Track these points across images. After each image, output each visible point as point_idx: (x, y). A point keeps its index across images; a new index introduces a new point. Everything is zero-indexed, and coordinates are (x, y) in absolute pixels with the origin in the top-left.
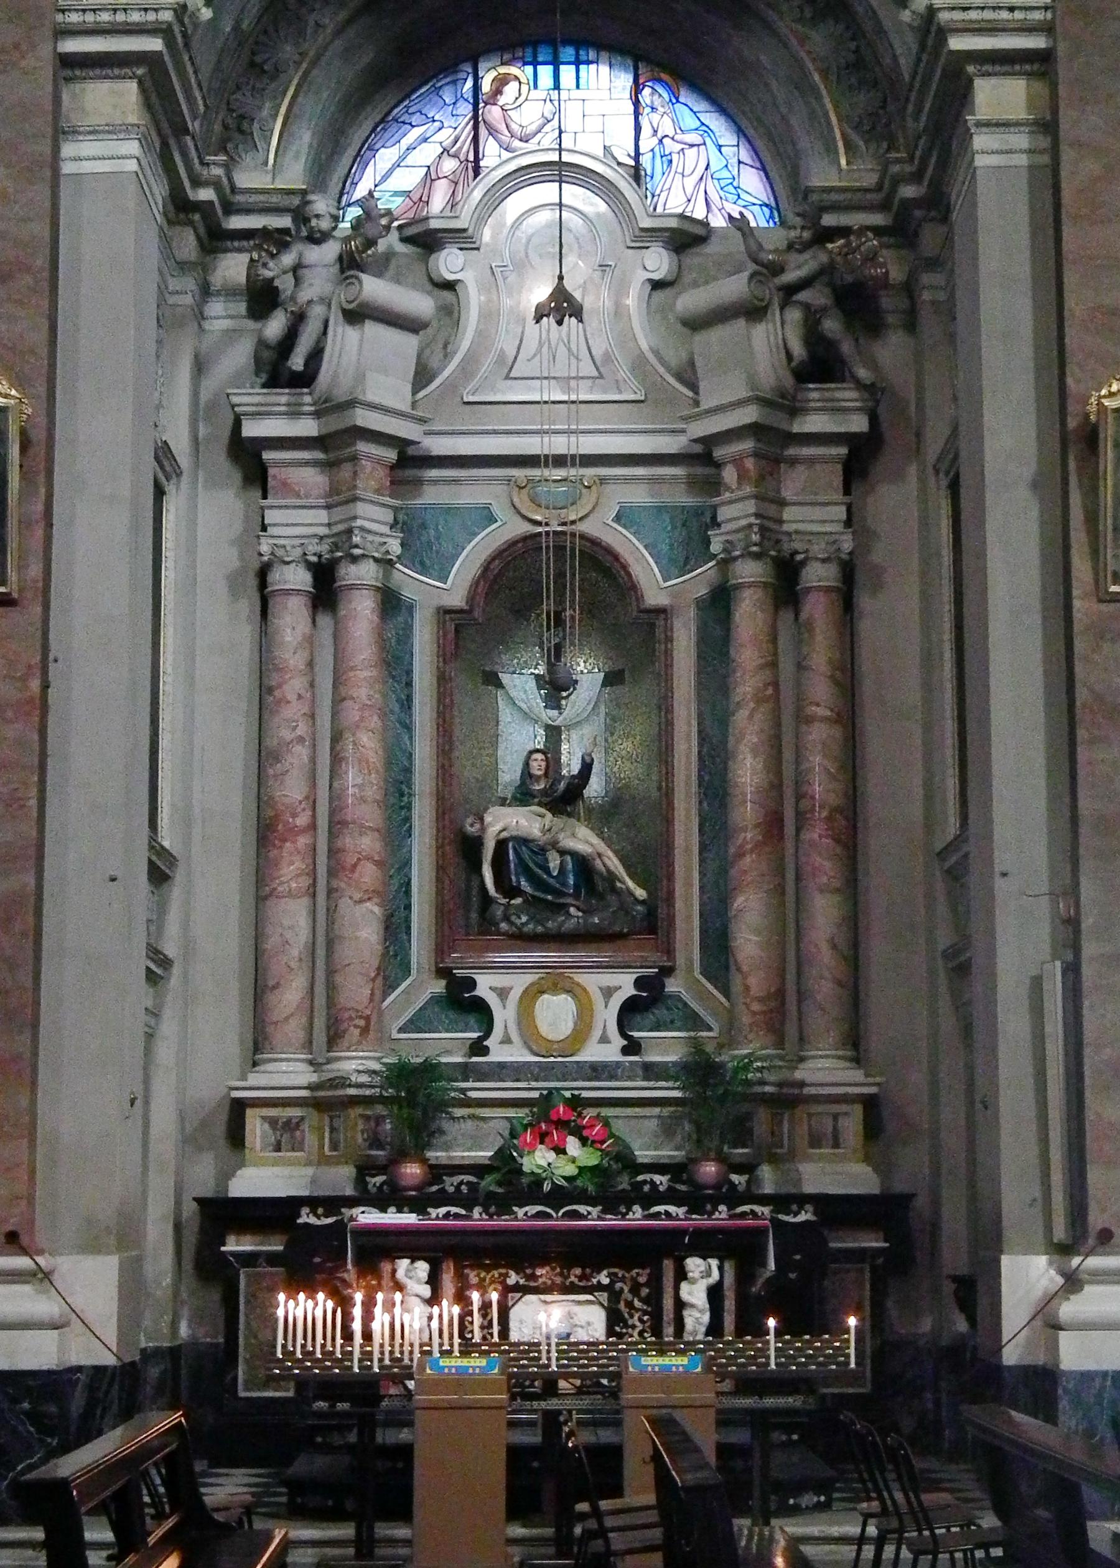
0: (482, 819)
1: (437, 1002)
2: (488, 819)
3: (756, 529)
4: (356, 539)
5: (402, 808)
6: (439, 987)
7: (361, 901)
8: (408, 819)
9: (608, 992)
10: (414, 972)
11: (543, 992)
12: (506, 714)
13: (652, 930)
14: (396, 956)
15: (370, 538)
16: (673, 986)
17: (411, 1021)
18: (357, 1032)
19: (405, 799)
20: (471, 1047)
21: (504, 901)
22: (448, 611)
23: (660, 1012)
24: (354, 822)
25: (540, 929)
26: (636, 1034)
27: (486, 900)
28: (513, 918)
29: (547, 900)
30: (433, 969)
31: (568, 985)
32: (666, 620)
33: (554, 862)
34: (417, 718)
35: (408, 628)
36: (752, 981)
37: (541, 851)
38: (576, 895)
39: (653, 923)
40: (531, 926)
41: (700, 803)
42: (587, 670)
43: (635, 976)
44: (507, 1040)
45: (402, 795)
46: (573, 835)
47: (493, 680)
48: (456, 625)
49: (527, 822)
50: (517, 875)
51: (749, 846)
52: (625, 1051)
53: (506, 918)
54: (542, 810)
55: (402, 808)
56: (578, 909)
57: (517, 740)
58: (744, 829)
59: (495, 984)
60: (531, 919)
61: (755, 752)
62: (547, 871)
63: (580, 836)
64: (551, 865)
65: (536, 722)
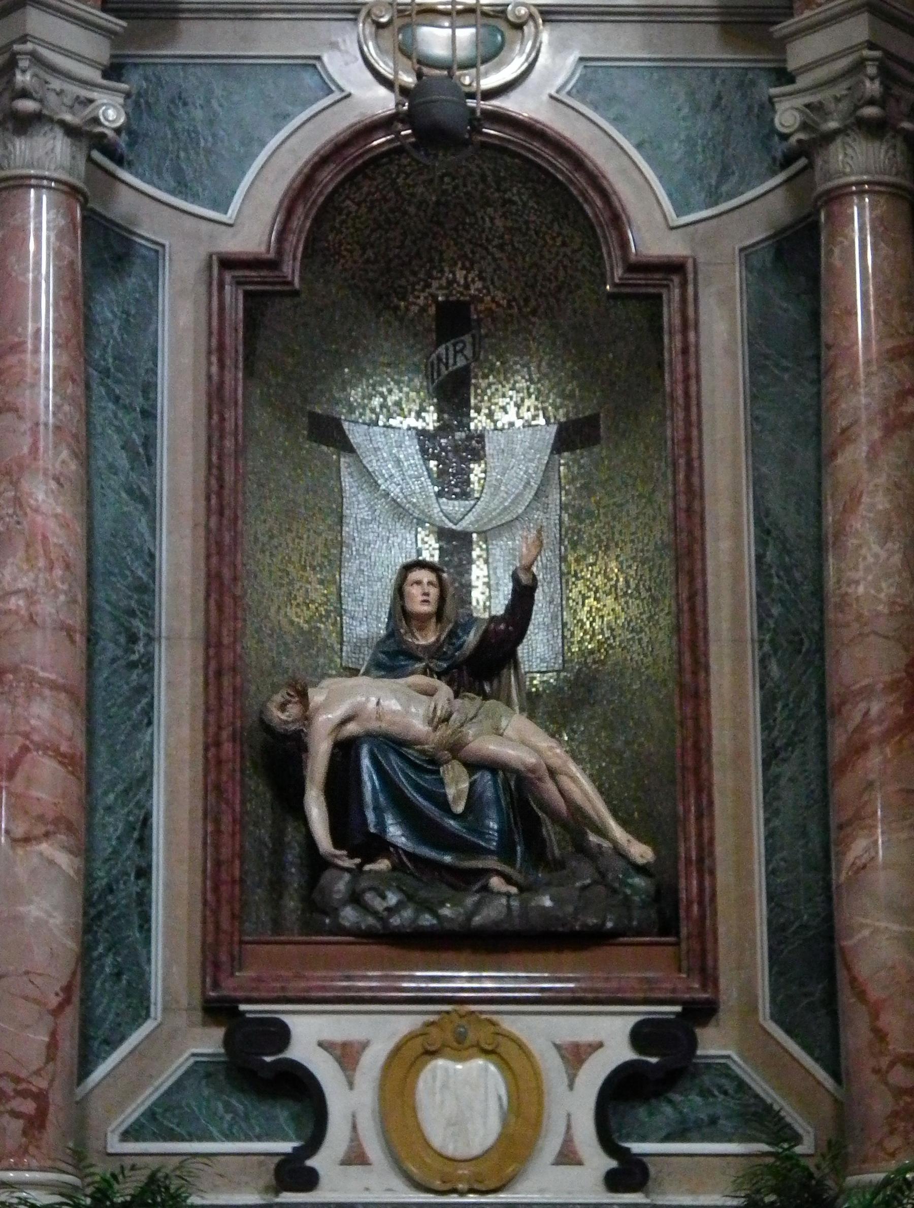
0: (303, 696)
1: (208, 1075)
2: (317, 697)
3: (872, 70)
4: (23, 79)
5: (132, 665)
6: (209, 1042)
7: (27, 840)
8: (145, 690)
9: (575, 1055)
10: (156, 1010)
11: (432, 1054)
12: (358, 505)
13: (668, 926)
14: (118, 975)
15: (56, 84)
16: (714, 1044)
17: (151, 1114)
18: (17, 1125)
19: (140, 647)
20: (279, 1168)
21: (348, 863)
22: (228, 263)
23: (690, 1103)
24: (15, 670)
25: (427, 920)
26: (637, 1147)
27: (316, 863)
28: (369, 896)
29: (443, 857)
30: (197, 1001)
31: (483, 1035)
32: (684, 285)
33: (457, 785)
34: (164, 485)
35: (150, 298)
36: (892, 1022)
37: (429, 765)
38: (506, 852)
39: (668, 913)
40: (408, 913)
41: (763, 662)
42: (515, 416)
43: (632, 1021)
44: (356, 1157)
45: (133, 639)
46: (498, 732)
47: (330, 433)
48: (253, 291)
49: (402, 705)
50: (377, 809)
51: (875, 730)
52: (613, 1182)
53: (355, 899)
54: (435, 682)
55: (132, 665)
56: (509, 880)
57: (381, 552)
58: (867, 692)
59: (327, 1036)
60: (409, 898)
61: (886, 534)
62: (443, 804)
63: (509, 732)
64: (451, 792)
65: (420, 522)
